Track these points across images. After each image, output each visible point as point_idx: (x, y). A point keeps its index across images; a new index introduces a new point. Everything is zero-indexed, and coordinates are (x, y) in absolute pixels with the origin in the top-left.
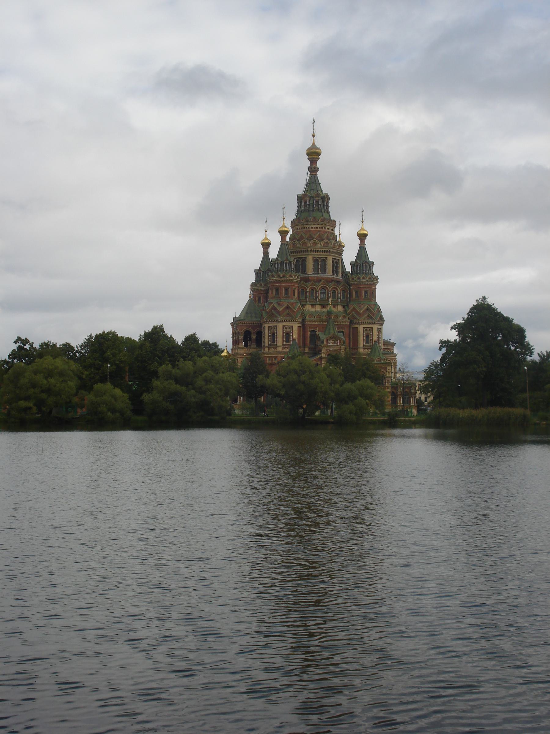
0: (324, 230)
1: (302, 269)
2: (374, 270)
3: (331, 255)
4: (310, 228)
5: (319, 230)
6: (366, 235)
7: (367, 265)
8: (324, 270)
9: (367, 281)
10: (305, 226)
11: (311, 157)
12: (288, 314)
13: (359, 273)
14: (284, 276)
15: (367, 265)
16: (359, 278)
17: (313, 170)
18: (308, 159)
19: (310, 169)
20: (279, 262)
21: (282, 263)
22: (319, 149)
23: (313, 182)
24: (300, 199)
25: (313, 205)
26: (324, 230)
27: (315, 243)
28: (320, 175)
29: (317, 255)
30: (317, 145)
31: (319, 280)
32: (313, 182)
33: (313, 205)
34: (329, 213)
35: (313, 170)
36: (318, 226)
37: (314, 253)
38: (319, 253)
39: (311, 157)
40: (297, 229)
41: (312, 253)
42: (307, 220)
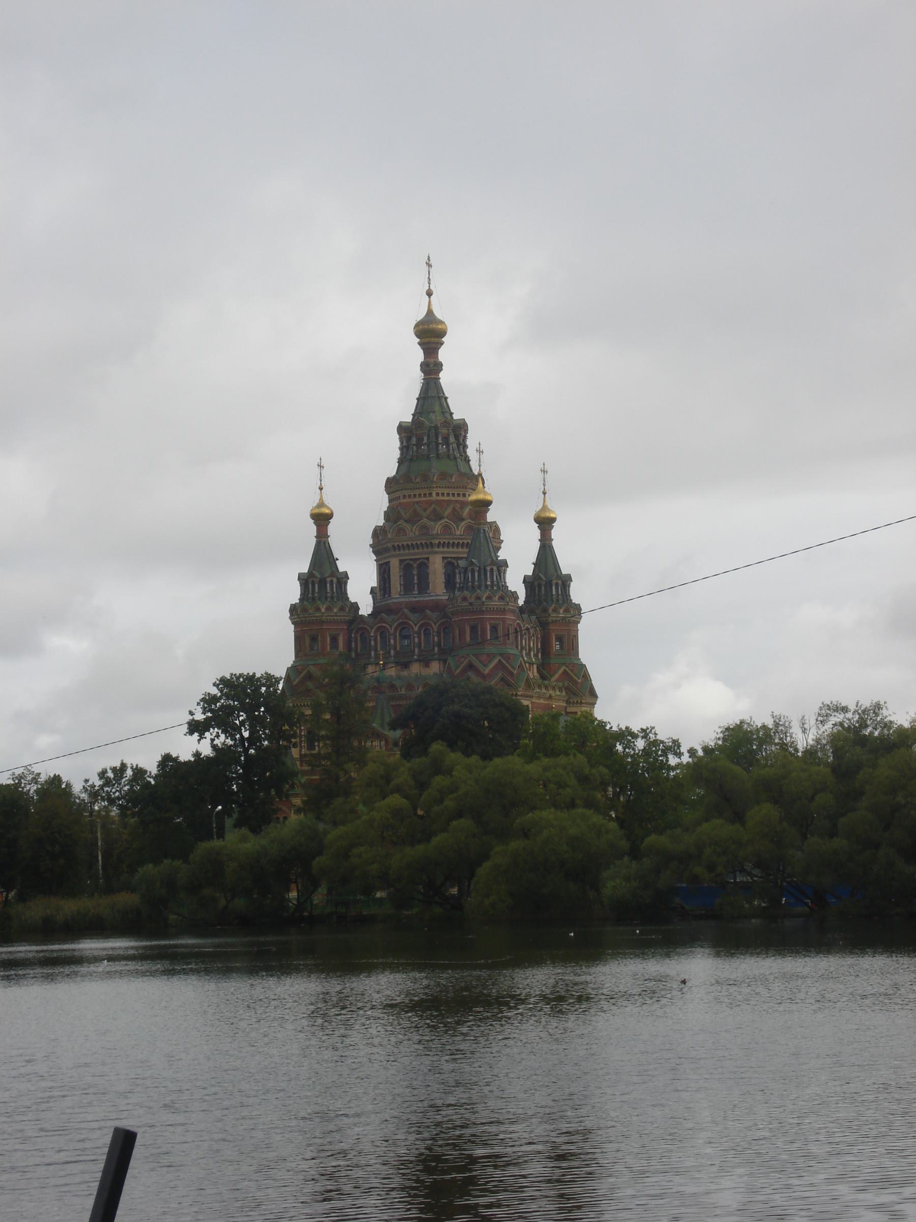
0: (428, 498)
1: (419, 584)
2: (507, 581)
3: (437, 553)
4: (434, 494)
5: (417, 499)
6: (329, 517)
7: (495, 568)
8: (424, 586)
9: (471, 604)
10: (422, 492)
11: (426, 340)
12: (502, 679)
13: (479, 587)
14: (328, 609)
15: (495, 568)
16: (478, 598)
17: (431, 369)
18: (420, 344)
19: (439, 367)
20: (317, 580)
21: (322, 582)
22: (442, 322)
23: (431, 395)
24: (403, 430)
25: (433, 442)
26: (428, 498)
27: (446, 527)
28: (444, 378)
29: (452, 552)
30: (438, 314)
31: (415, 608)
32: (431, 395)
33: (433, 442)
34: (469, 461)
35: (431, 369)
36: (417, 492)
37: (446, 549)
38: (455, 550)
39: (426, 340)
40: (404, 497)
41: (441, 549)
42: (425, 478)
